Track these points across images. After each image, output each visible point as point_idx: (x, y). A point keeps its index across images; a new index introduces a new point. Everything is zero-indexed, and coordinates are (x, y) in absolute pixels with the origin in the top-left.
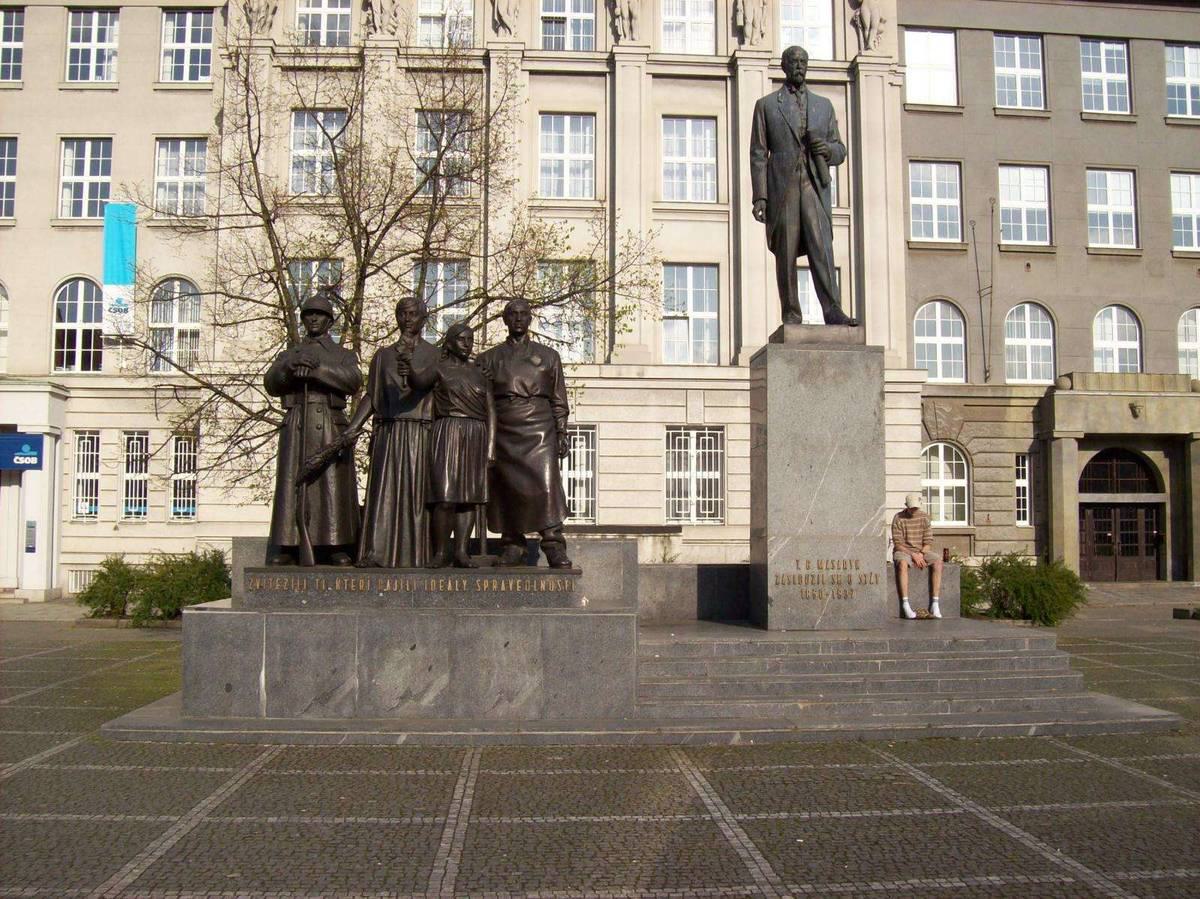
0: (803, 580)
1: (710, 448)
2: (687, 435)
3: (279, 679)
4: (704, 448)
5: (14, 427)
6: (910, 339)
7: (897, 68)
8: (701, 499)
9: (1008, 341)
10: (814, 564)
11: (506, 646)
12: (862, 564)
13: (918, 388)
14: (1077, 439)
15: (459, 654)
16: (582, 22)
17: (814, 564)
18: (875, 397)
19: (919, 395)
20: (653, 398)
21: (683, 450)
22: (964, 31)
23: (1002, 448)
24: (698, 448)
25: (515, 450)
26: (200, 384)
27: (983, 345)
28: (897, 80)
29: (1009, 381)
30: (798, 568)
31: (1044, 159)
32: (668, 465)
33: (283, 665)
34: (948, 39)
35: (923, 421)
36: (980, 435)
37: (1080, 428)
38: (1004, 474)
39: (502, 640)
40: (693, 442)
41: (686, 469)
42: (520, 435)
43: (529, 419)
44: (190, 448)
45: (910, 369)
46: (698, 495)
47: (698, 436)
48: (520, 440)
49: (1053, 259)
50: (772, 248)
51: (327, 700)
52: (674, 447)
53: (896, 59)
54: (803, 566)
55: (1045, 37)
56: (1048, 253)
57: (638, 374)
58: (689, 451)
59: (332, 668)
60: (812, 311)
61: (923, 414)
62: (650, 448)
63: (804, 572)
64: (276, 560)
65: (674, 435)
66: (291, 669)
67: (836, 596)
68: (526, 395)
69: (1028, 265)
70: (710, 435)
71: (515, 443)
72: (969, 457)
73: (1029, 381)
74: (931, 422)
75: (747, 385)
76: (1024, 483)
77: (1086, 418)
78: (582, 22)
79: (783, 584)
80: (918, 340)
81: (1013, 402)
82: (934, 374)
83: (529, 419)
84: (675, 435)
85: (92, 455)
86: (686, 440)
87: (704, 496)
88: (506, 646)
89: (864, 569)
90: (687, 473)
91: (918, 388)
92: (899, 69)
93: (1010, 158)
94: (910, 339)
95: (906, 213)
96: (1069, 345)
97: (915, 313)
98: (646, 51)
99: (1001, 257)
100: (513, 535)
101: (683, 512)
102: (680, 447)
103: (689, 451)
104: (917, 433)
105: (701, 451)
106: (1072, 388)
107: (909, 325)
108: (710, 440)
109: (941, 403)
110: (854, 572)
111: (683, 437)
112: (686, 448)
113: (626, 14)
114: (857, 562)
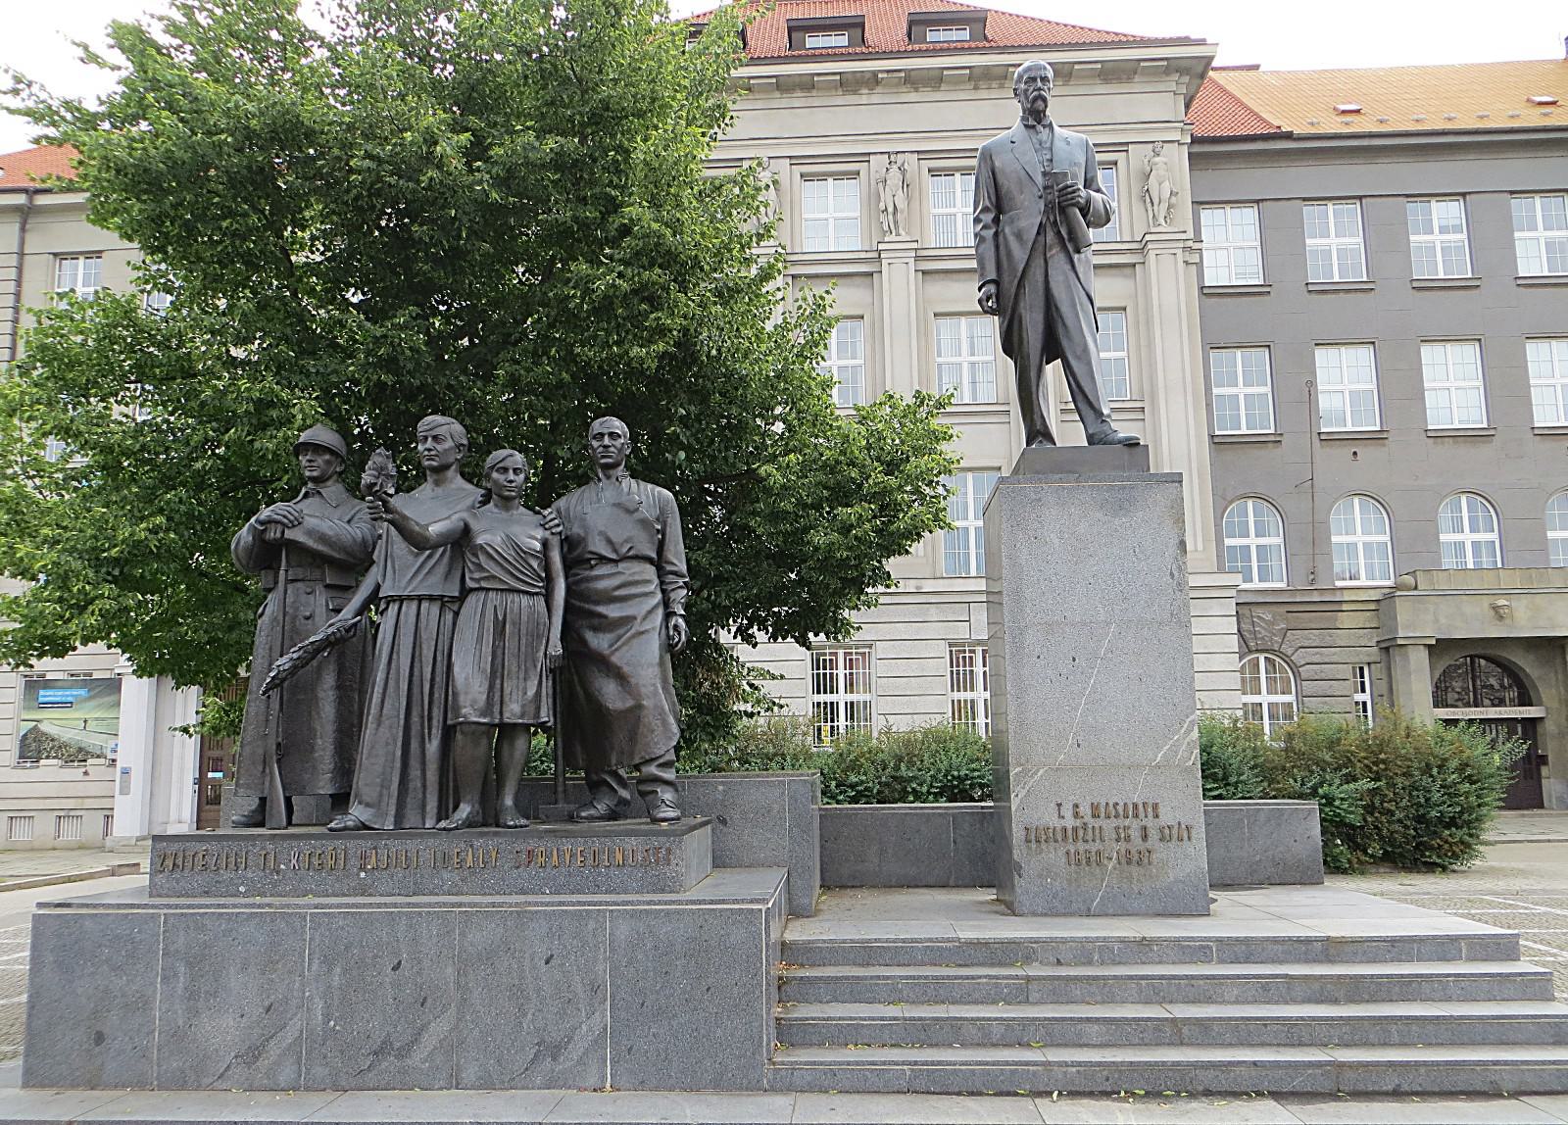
0: (1070, 832)
2: (974, 652)
3: (180, 1023)
6: (1219, 541)
7: (1192, 248)
9: (1334, 539)
10: (1085, 810)
11: (547, 963)
12: (1161, 811)
13: (1233, 593)
14: (1429, 646)
15: (471, 977)
17: (1085, 810)
18: (1172, 549)
19: (1234, 601)
20: (933, 613)
22: (1268, 202)
23: (1335, 659)
25: (599, 642)
27: (1309, 541)
28: (1196, 258)
29: (1339, 584)
30: (1062, 817)
31: (1369, 336)
32: (952, 686)
33: (189, 999)
34: (1250, 214)
35: (1239, 631)
36: (1306, 645)
37: (1431, 632)
38: (1337, 688)
42: (605, 617)
43: (617, 593)
44: (960, 716)
45: (1221, 570)
48: (604, 625)
49: (1384, 445)
50: (1008, 349)
51: (256, 1058)
53: (1191, 235)
54: (1068, 812)
55: (1364, 201)
56: (1376, 438)
57: (917, 588)
59: (267, 1004)
60: (1069, 433)
61: (1239, 623)
62: (931, 667)
63: (1070, 822)
66: (201, 1004)
67: (1123, 861)
68: (613, 556)
69: (1355, 453)
71: (596, 629)
72: (1295, 670)
73: (1363, 582)
74: (1249, 631)
76: (1366, 697)
77: (1437, 621)
79: (1038, 841)
80: (1228, 542)
81: (1345, 607)
82: (1248, 579)
83: (617, 593)
86: (971, 658)
88: (547, 963)
89: (1167, 817)
91: (1233, 593)
92: (1197, 246)
93: (1325, 337)
94: (1219, 541)
95: (1209, 405)
96: (1414, 541)
97: (1224, 511)
98: (914, 245)
99: (1322, 447)
104: (1234, 642)
106: (1416, 588)
107: (1218, 526)
109: (1259, 611)
110: (1150, 822)
112: (971, 665)
113: (890, 209)
114: (1155, 806)
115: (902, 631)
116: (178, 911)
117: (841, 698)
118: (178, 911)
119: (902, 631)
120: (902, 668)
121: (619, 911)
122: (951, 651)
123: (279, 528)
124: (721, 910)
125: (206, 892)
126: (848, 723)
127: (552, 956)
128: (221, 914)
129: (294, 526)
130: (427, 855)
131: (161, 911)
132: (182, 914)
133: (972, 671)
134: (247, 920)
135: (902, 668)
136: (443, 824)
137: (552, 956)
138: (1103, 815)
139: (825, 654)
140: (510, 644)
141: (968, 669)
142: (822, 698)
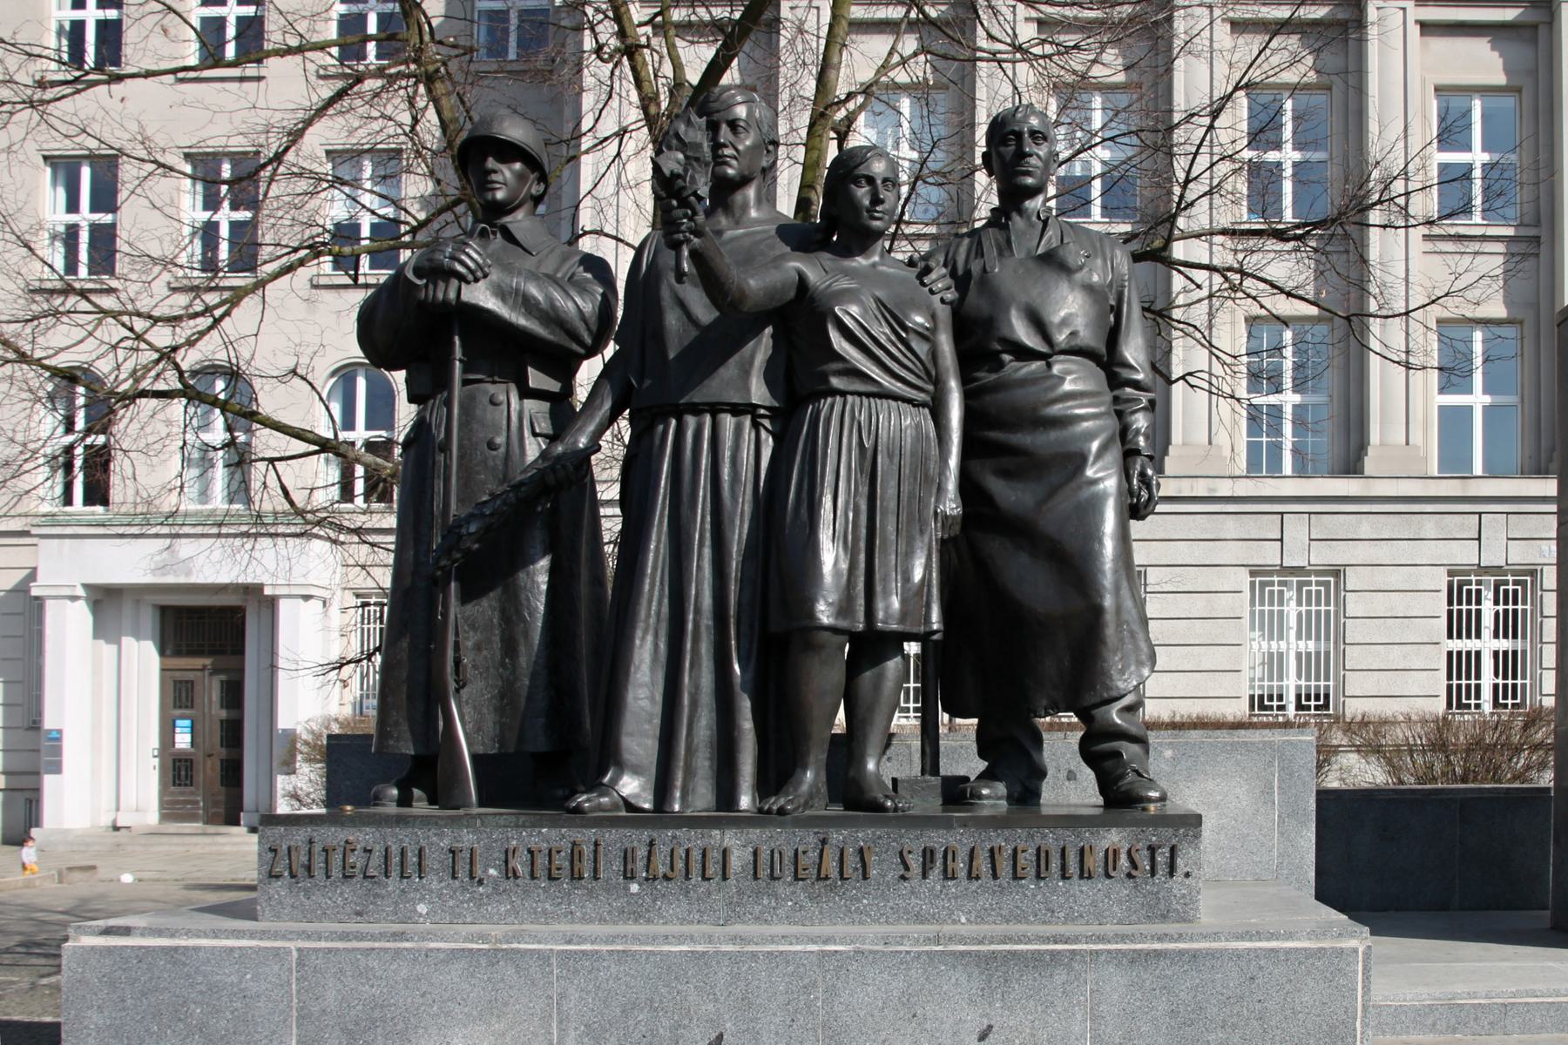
1: (1318, 603)
4: (1309, 603)
5: (57, 768)
8: (1500, 681)
16: (514, 21)
20: (1231, 527)
21: (1276, 608)
24: (1496, 602)
26: (93, 298)
39: (974, 1020)
40: (1488, 595)
41: (1281, 638)
46: (1299, 677)
47: (1300, 585)
52: (1262, 603)
58: (1285, 608)
64: (183, 740)
65: (1263, 585)
70: (1515, 583)
75: (1554, 508)
78: (514, 21)
84: (1460, 591)
85: (1469, 611)
87: (1505, 677)
90: (1283, 644)
100: (1013, 756)
101: (1473, 702)
102: (1271, 603)
103: (1285, 608)
105: (1304, 608)
108: (1318, 592)
111: (1276, 588)
115: (1182, 552)
116: (323, 944)
117: (1488, 644)
118: (323, 944)
119: (1182, 552)
120: (1183, 606)
121: (1109, 951)
122: (1252, 584)
123: (454, 283)
124: (1288, 951)
125: (359, 914)
126: (1500, 681)
127: (990, 1027)
128: (398, 952)
129: (477, 280)
130: (739, 859)
131: (292, 945)
132: (330, 950)
133: (1281, 613)
134: (446, 962)
135: (1183, 606)
136: (775, 803)
137: (990, 1027)
138: (963, 874)
139: (1470, 582)
140: (887, 491)
141: (1276, 608)
142: (1457, 645)
